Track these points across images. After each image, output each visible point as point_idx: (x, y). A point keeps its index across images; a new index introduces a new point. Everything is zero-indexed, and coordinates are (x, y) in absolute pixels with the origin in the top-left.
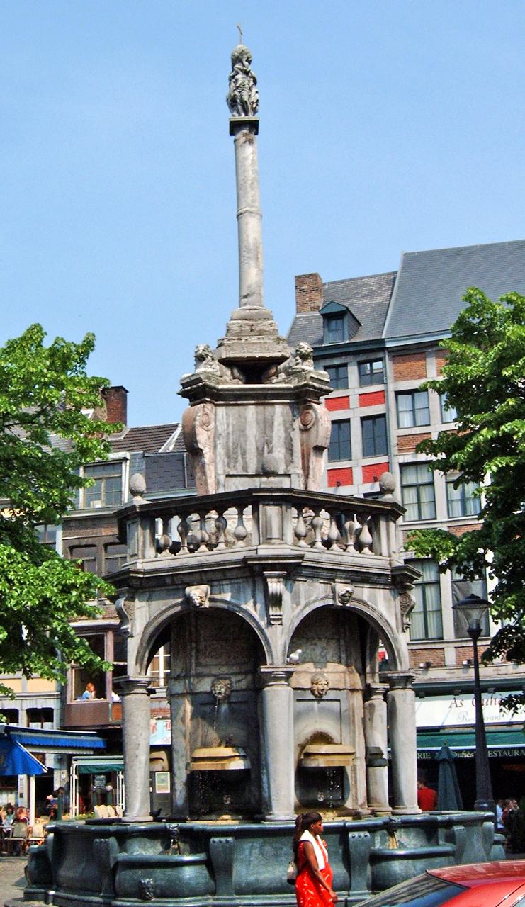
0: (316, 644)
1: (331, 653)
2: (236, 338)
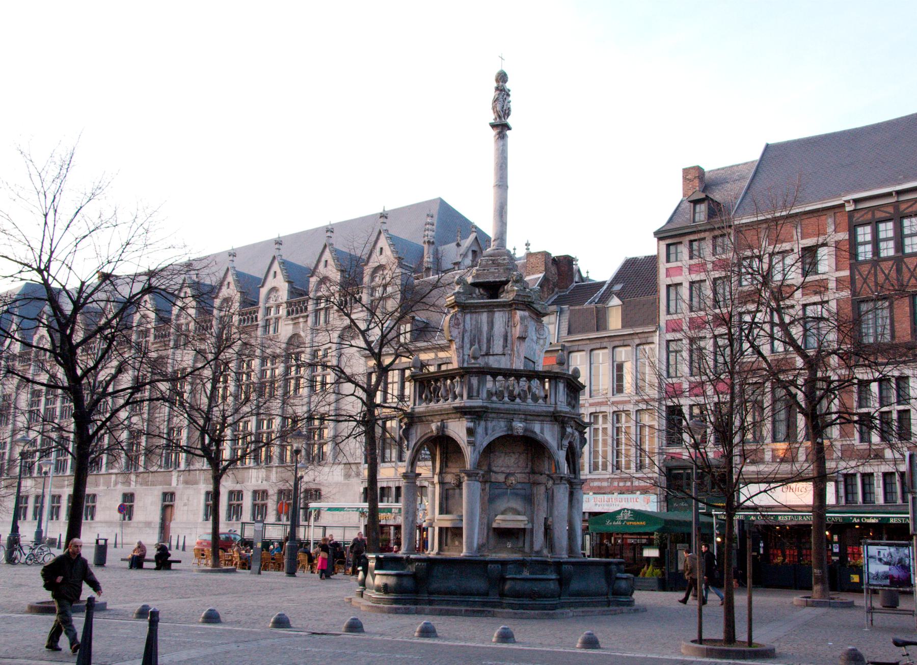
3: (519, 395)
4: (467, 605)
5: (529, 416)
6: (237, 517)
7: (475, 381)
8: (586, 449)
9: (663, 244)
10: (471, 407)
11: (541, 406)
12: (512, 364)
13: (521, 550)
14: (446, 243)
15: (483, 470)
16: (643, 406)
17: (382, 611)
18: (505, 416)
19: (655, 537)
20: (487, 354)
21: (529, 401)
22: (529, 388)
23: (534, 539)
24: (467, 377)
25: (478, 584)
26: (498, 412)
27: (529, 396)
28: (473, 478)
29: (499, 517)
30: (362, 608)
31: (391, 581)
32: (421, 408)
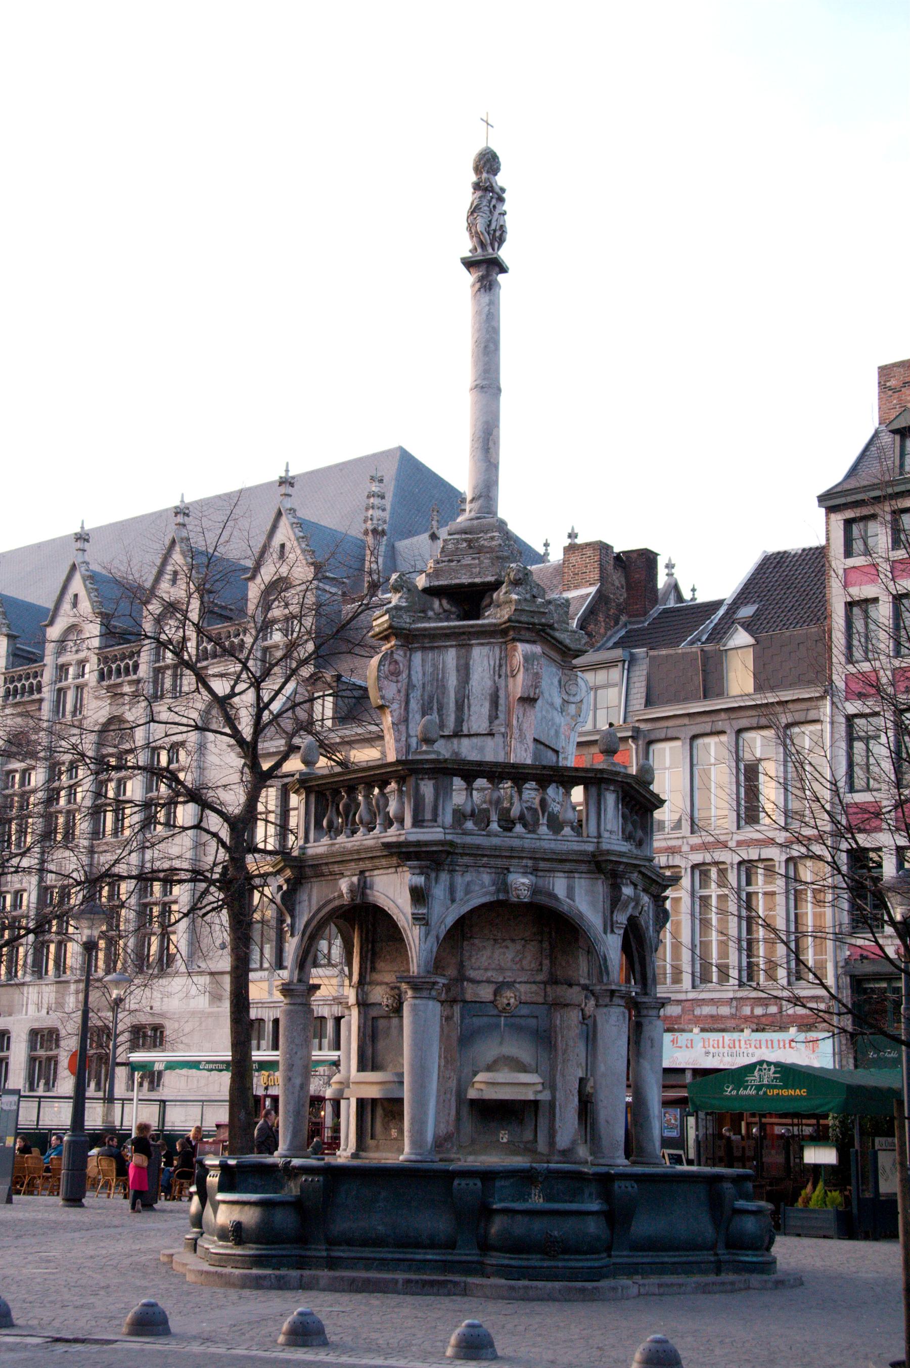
0: (507, 947)
1: (529, 958)
2: (446, 559)
3: (522, 818)
4: (409, 1270)
5: (542, 862)
6: (47, 1084)
7: (427, 788)
9: (838, 520)
10: (418, 844)
11: (568, 842)
12: (508, 754)
13: (530, 1149)
14: (410, 534)
15: (447, 979)
16: (798, 850)
17: (227, 1282)
18: (493, 862)
19: (830, 1122)
20: (457, 734)
21: (543, 829)
22: (543, 803)
23: (558, 1124)
24: (411, 781)
25: (434, 1222)
26: (476, 853)
27: (543, 820)
28: (425, 994)
29: (480, 1077)
30: (190, 1278)
31: (249, 1217)
32: (320, 847)
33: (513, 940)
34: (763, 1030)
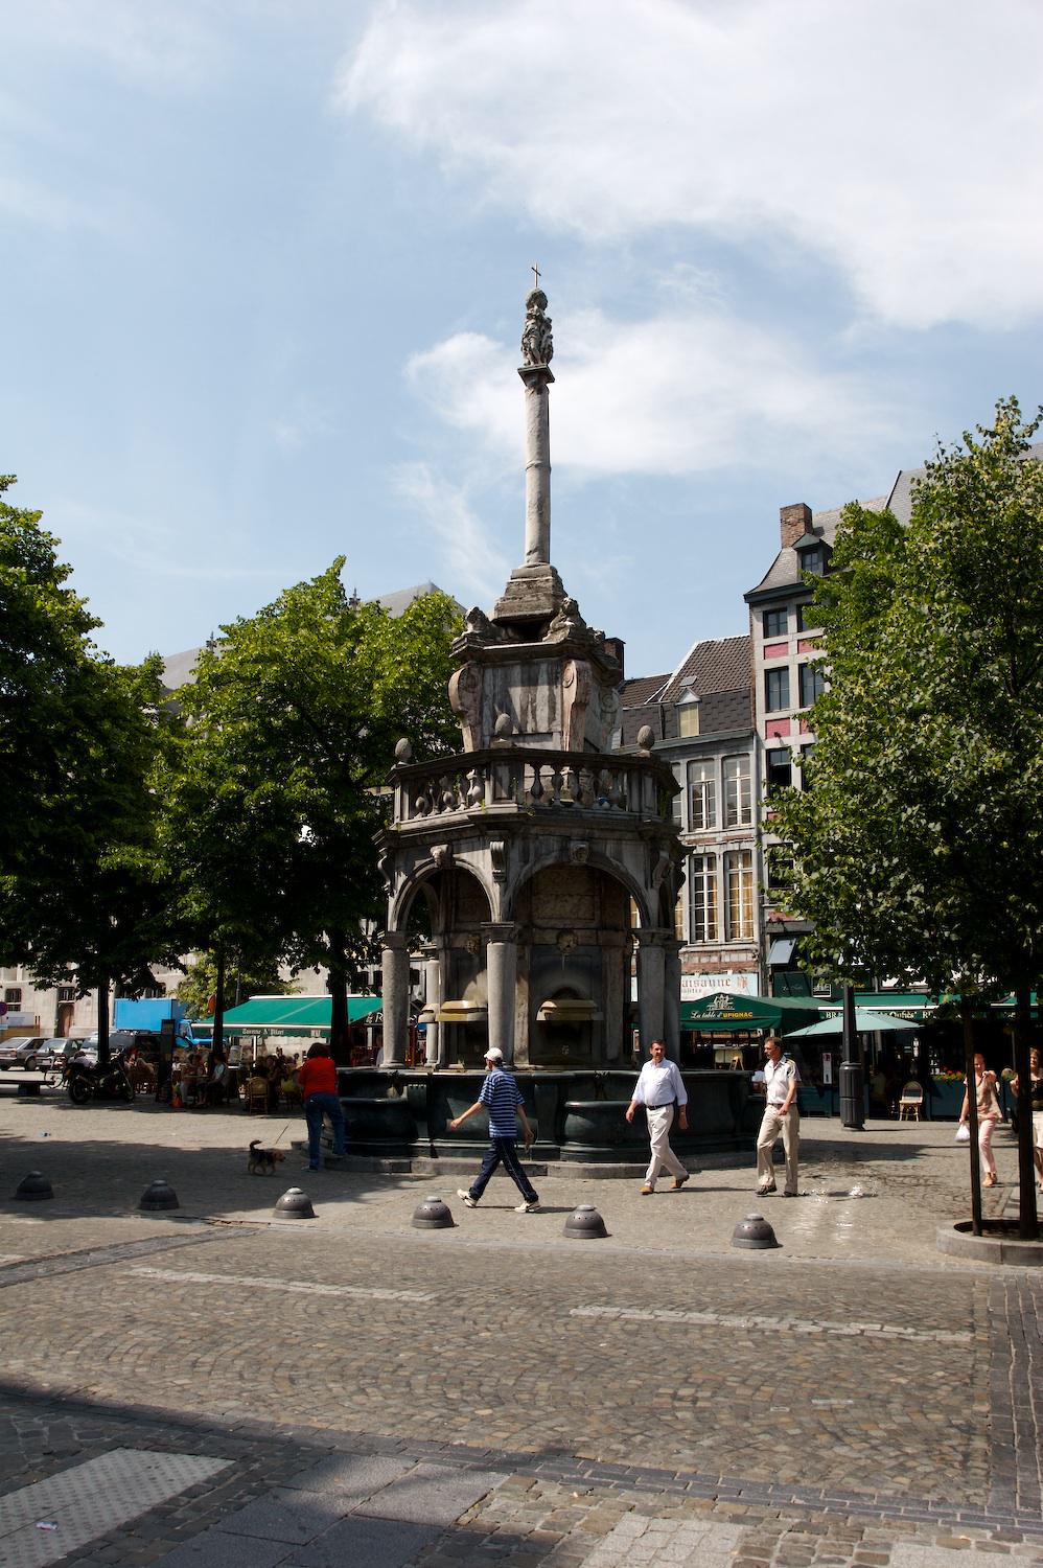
8: (685, 888)
33: (571, 895)
34: (707, 974)
